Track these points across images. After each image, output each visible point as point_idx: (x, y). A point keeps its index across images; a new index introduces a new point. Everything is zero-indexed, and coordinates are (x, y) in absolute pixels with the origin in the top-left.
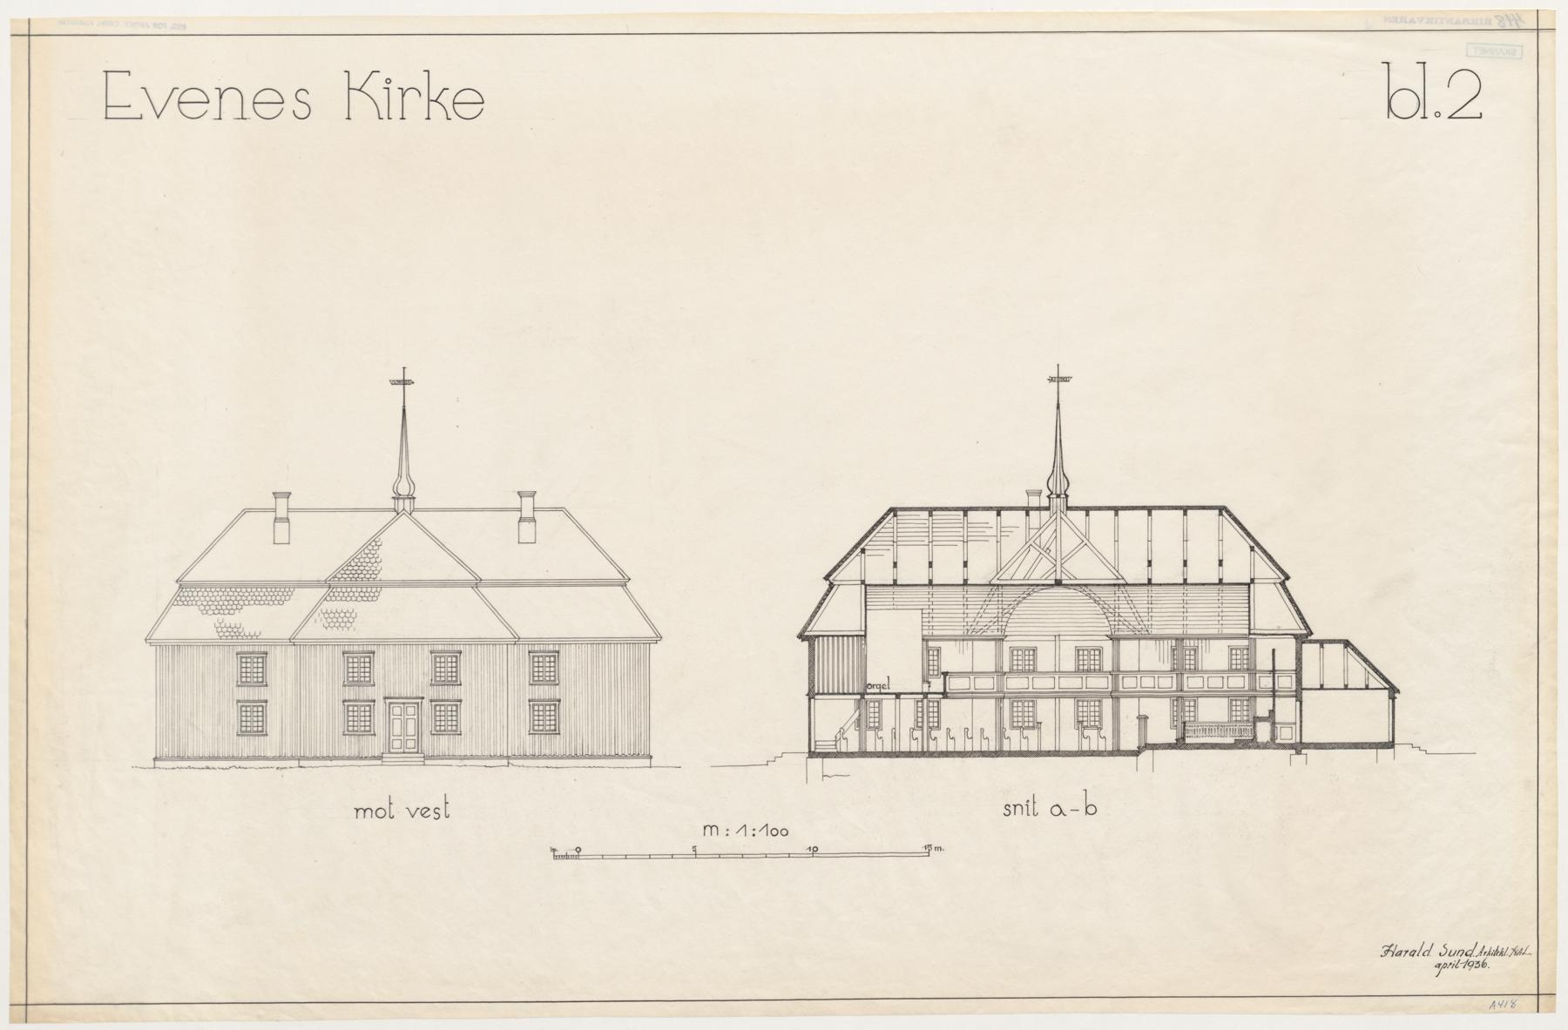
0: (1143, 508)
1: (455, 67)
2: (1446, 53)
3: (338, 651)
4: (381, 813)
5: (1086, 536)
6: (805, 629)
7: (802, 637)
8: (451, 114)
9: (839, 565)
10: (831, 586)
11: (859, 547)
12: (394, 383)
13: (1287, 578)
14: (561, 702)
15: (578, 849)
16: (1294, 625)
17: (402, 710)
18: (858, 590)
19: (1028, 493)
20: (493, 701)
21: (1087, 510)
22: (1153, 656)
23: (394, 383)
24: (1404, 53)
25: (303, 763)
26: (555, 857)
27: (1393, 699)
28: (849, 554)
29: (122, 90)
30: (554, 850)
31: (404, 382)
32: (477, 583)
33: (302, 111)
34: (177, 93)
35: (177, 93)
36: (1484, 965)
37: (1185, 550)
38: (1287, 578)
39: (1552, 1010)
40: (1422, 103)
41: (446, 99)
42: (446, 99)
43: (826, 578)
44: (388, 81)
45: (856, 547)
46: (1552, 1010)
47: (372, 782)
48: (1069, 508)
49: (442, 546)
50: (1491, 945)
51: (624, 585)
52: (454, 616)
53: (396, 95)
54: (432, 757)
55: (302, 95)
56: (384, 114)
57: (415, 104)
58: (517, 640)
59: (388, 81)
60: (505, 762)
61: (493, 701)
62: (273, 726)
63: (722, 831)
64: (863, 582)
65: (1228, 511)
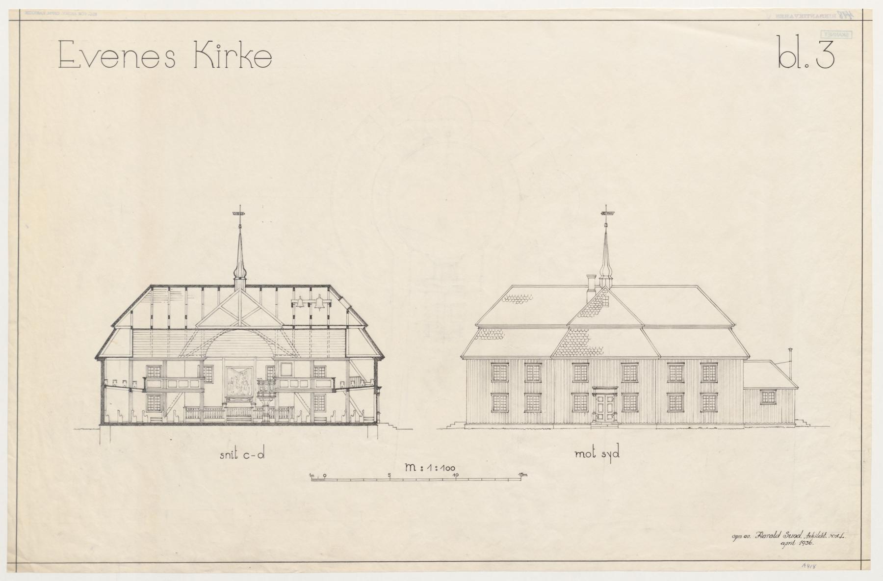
0: (199, 286)
1: (254, 39)
2: (811, 33)
3: (619, 362)
4: (588, 455)
5: (261, 303)
6: (99, 353)
7: (97, 358)
8: (254, 65)
9: (121, 317)
10: (115, 329)
11: (129, 310)
12: (234, 214)
13: (366, 325)
14: (356, 393)
15: (325, 475)
16: (373, 352)
17: (607, 395)
18: (128, 332)
19: (588, 276)
20: (653, 390)
21: (261, 287)
22: (303, 369)
23: (234, 214)
24: (788, 30)
25: (659, 427)
26: (313, 480)
27: (377, 394)
28: (124, 313)
29: (70, 52)
30: (311, 476)
31: (241, 214)
32: (643, 327)
33: (170, 63)
34: (100, 54)
35: (100, 54)
36: (809, 543)
37: (152, 310)
38: (366, 325)
39: (869, 569)
40: (797, 59)
41: (251, 57)
42: (251, 57)
43: (113, 326)
44: (218, 46)
45: (128, 309)
46: (869, 569)
47: (583, 438)
48: (247, 286)
49: (715, 305)
50: (815, 530)
51: (731, 328)
52: (629, 344)
53: (223, 54)
54: (621, 424)
55: (170, 55)
56: (216, 65)
57: (233, 59)
58: (660, 357)
59: (218, 46)
60: (742, 427)
61: (653, 390)
62: (687, 407)
63: (418, 468)
64: (132, 328)
65: (333, 289)
